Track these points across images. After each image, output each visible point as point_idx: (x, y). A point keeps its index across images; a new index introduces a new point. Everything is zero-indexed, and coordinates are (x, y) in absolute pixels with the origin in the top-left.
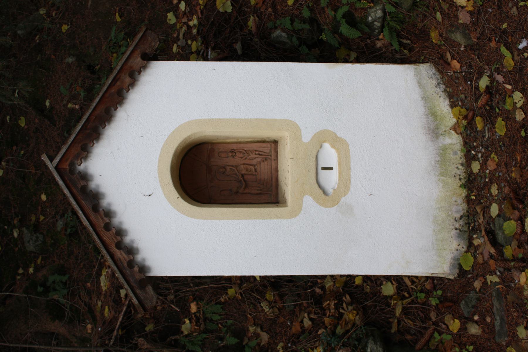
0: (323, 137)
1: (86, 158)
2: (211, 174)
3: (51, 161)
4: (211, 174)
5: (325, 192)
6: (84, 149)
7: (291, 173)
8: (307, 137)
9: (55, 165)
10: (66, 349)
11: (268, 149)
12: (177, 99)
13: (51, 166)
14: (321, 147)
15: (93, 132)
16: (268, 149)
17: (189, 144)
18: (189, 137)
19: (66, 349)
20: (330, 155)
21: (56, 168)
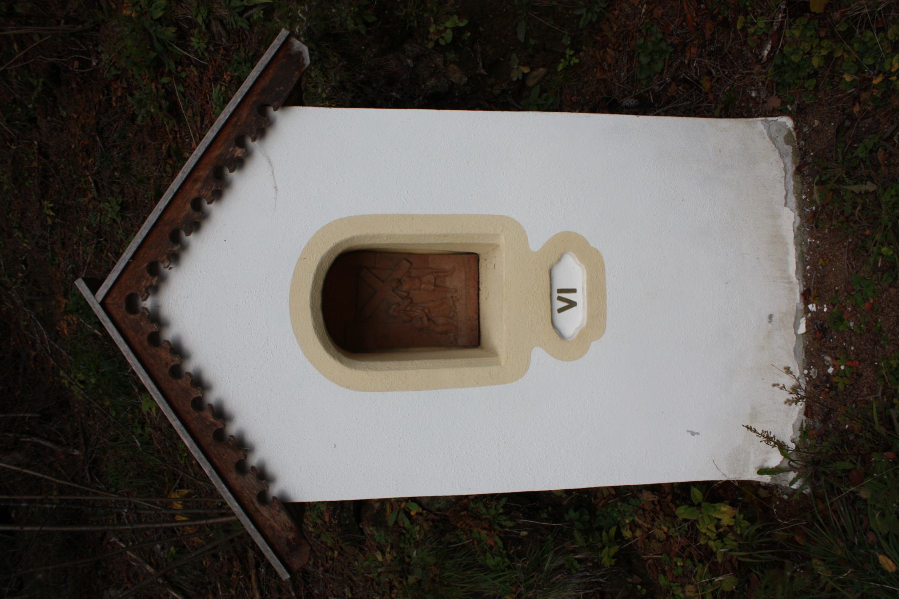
0: (566, 243)
1: (155, 289)
2: (383, 304)
3: (94, 291)
4: (383, 304)
5: (561, 336)
6: (153, 269)
7: (503, 305)
8: (536, 243)
9: (100, 299)
10: (84, 529)
11: (465, 265)
12: (331, 172)
13: (94, 301)
14: (559, 260)
15: (170, 244)
16: (465, 265)
17: (326, 266)
18: (352, 239)
19: (84, 529)
20: (572, 273)
21: (103, 304)
